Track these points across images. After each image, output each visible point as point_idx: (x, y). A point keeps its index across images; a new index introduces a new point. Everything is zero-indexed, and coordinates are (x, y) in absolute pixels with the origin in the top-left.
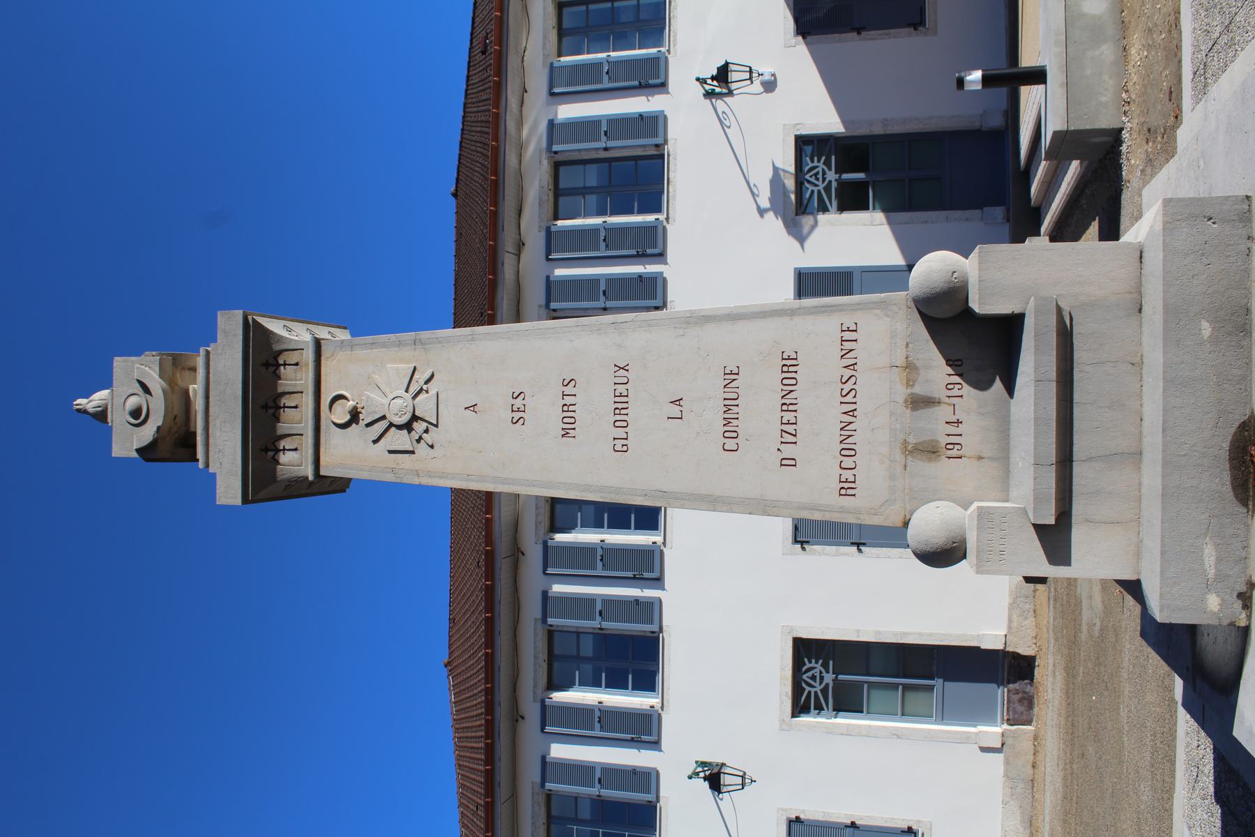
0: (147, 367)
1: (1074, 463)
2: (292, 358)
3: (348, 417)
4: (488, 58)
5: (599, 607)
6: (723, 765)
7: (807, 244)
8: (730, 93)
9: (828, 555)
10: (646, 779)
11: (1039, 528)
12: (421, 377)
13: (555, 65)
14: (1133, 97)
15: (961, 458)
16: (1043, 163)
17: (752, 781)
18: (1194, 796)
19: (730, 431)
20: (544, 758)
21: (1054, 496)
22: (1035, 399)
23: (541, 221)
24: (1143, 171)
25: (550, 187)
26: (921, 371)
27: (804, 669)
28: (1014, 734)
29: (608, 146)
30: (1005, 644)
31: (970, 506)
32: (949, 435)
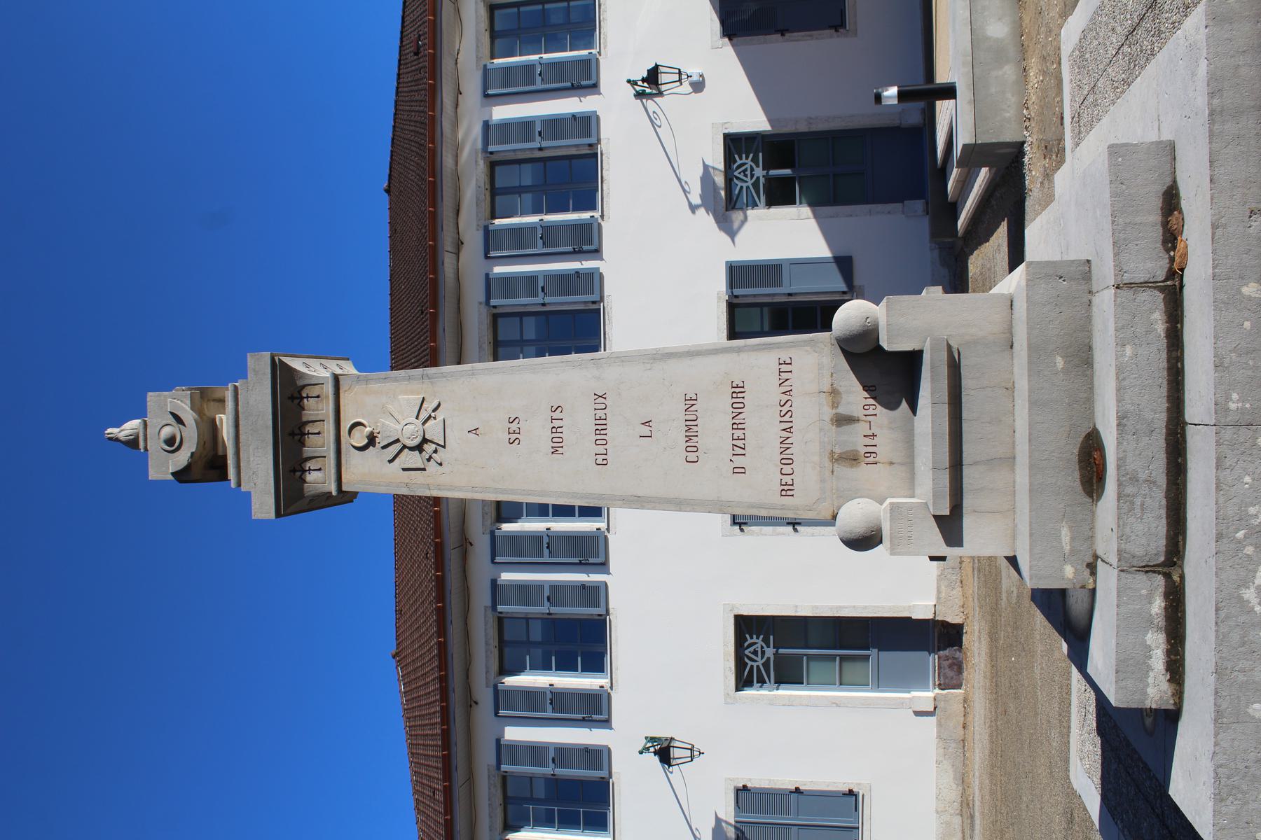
0: (180, 401)
1: (964, 467)
2: (314, 391)
3: (366, 441)
4: (421, 60)
5: (546, 593)
6: (672, 739)
7: (737, 239)
8: (660, 94)
9: (766, 535)
10: (598, 756)
11: (938, 519)
12: (429, 406)
13: (488, 68)
14: (1033, 115)
15: (876, 463)
16: (955, 171)
17: (700, 753)
18: (1084, 732)
19: (692, 448)
20: (498, 741)
21: (948, 493)
22: (932, 417)
23: (479, 220)
24: (1042, 183)
25: (487, 187)
26: (843, 396)
27: (746, 644)
28: (945, 697)
29: (542, 146)
30: (935, 614)
31: (884, 501)
32: (866, 446)
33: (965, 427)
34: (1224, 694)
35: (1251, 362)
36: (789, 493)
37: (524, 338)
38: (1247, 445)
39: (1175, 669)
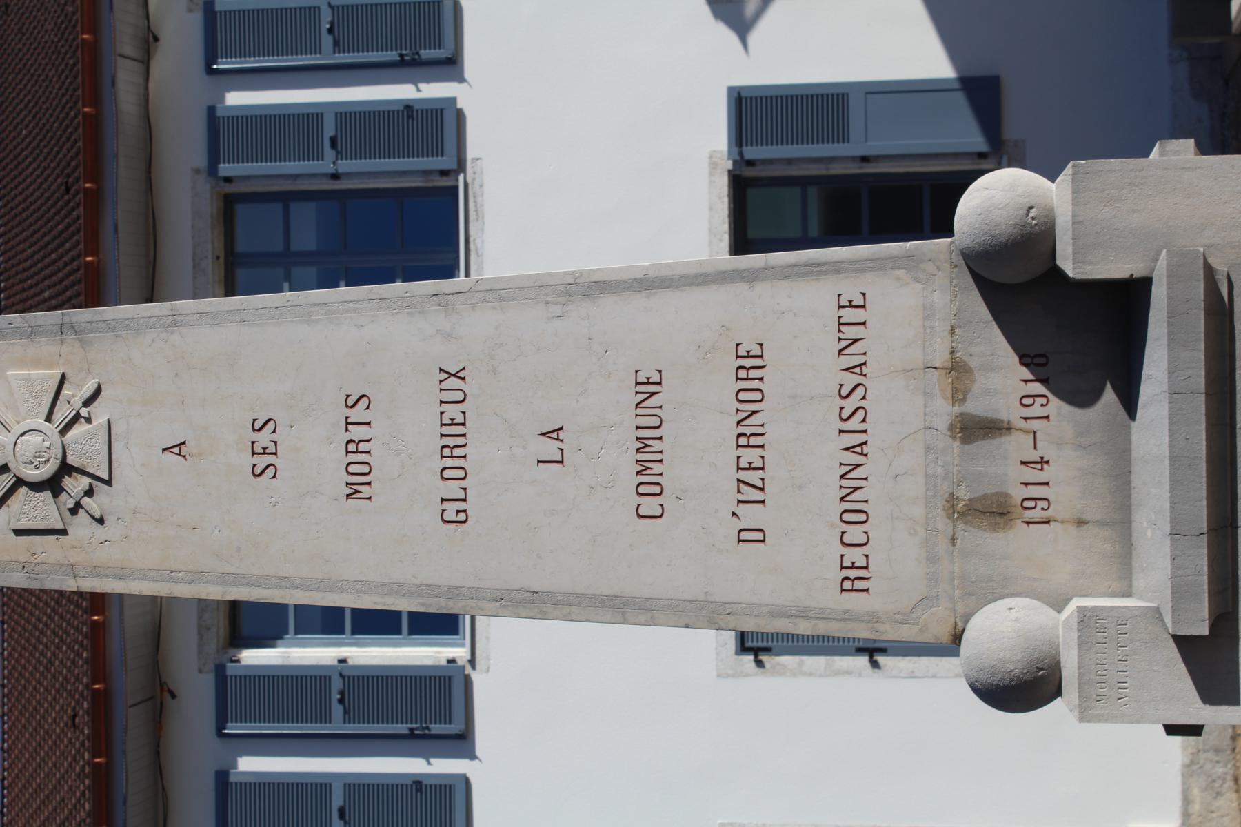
11: (1184, 643)
12: (75, 394)
29: (340, 170)
36: (860, 585)
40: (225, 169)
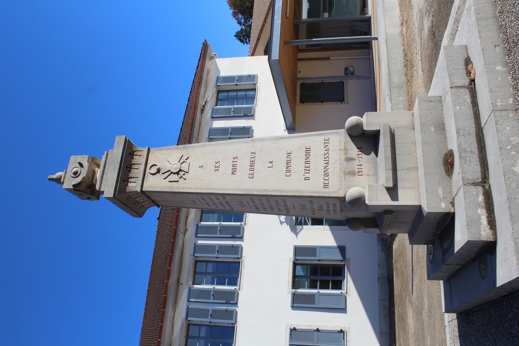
0: (84, 160)
7: (298, 236)
11: (388, 189)
12: (184, 158)
19: (288, 171)
26: (349, 151)
29: (218, 256)
33: (397, 157)
34: (513, 208)
35: (503, 90)
36: (327, 187)
37: (200, 336)
38: (506, 117)
39: (492, 223)
40: (196, 255)
